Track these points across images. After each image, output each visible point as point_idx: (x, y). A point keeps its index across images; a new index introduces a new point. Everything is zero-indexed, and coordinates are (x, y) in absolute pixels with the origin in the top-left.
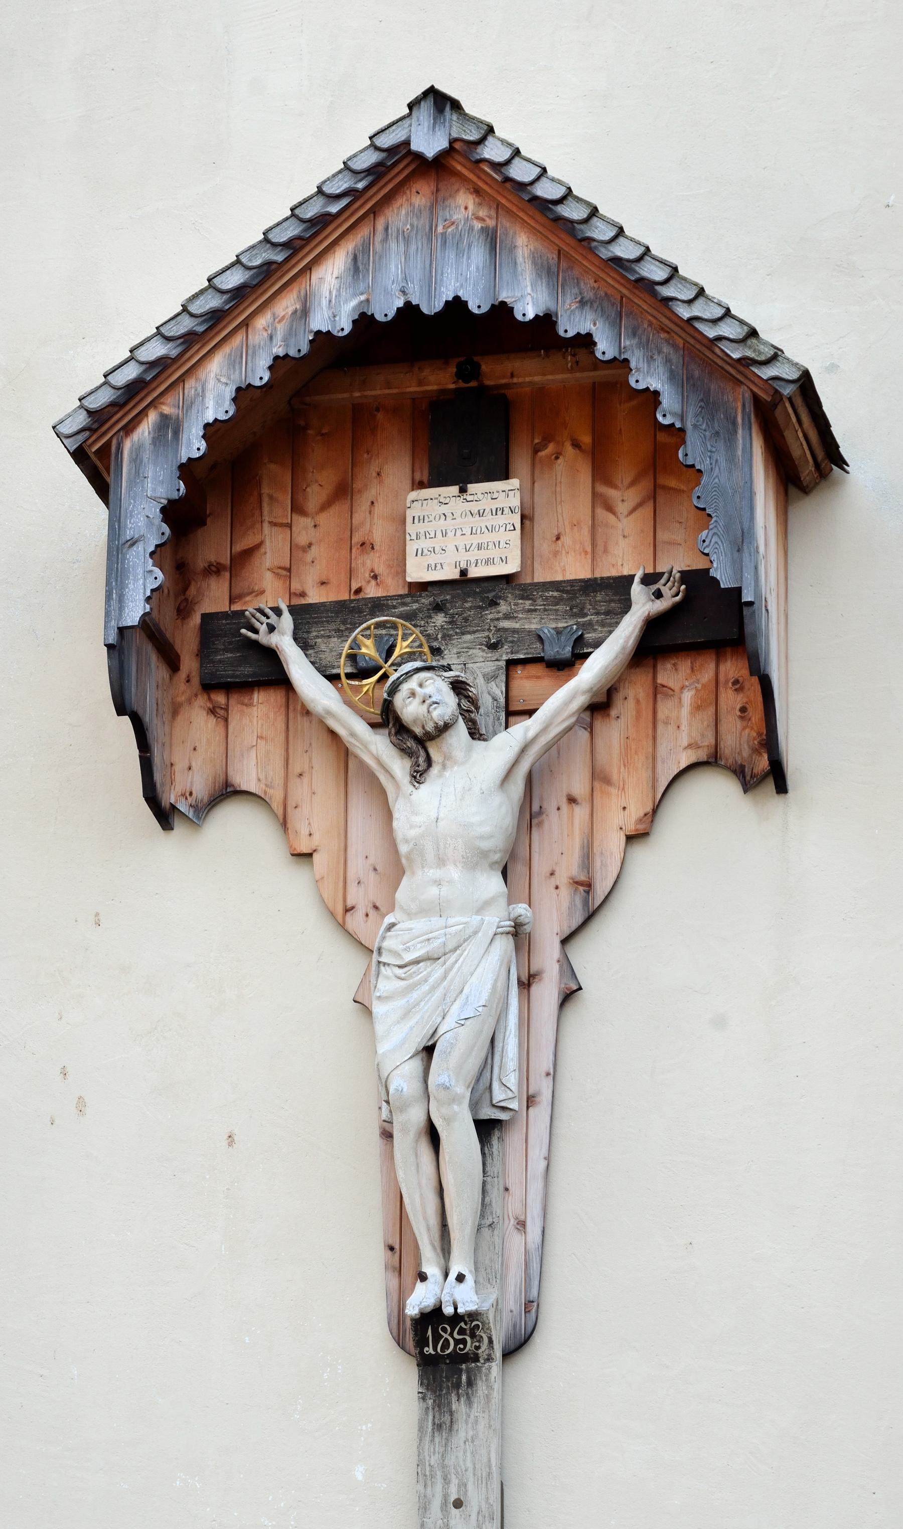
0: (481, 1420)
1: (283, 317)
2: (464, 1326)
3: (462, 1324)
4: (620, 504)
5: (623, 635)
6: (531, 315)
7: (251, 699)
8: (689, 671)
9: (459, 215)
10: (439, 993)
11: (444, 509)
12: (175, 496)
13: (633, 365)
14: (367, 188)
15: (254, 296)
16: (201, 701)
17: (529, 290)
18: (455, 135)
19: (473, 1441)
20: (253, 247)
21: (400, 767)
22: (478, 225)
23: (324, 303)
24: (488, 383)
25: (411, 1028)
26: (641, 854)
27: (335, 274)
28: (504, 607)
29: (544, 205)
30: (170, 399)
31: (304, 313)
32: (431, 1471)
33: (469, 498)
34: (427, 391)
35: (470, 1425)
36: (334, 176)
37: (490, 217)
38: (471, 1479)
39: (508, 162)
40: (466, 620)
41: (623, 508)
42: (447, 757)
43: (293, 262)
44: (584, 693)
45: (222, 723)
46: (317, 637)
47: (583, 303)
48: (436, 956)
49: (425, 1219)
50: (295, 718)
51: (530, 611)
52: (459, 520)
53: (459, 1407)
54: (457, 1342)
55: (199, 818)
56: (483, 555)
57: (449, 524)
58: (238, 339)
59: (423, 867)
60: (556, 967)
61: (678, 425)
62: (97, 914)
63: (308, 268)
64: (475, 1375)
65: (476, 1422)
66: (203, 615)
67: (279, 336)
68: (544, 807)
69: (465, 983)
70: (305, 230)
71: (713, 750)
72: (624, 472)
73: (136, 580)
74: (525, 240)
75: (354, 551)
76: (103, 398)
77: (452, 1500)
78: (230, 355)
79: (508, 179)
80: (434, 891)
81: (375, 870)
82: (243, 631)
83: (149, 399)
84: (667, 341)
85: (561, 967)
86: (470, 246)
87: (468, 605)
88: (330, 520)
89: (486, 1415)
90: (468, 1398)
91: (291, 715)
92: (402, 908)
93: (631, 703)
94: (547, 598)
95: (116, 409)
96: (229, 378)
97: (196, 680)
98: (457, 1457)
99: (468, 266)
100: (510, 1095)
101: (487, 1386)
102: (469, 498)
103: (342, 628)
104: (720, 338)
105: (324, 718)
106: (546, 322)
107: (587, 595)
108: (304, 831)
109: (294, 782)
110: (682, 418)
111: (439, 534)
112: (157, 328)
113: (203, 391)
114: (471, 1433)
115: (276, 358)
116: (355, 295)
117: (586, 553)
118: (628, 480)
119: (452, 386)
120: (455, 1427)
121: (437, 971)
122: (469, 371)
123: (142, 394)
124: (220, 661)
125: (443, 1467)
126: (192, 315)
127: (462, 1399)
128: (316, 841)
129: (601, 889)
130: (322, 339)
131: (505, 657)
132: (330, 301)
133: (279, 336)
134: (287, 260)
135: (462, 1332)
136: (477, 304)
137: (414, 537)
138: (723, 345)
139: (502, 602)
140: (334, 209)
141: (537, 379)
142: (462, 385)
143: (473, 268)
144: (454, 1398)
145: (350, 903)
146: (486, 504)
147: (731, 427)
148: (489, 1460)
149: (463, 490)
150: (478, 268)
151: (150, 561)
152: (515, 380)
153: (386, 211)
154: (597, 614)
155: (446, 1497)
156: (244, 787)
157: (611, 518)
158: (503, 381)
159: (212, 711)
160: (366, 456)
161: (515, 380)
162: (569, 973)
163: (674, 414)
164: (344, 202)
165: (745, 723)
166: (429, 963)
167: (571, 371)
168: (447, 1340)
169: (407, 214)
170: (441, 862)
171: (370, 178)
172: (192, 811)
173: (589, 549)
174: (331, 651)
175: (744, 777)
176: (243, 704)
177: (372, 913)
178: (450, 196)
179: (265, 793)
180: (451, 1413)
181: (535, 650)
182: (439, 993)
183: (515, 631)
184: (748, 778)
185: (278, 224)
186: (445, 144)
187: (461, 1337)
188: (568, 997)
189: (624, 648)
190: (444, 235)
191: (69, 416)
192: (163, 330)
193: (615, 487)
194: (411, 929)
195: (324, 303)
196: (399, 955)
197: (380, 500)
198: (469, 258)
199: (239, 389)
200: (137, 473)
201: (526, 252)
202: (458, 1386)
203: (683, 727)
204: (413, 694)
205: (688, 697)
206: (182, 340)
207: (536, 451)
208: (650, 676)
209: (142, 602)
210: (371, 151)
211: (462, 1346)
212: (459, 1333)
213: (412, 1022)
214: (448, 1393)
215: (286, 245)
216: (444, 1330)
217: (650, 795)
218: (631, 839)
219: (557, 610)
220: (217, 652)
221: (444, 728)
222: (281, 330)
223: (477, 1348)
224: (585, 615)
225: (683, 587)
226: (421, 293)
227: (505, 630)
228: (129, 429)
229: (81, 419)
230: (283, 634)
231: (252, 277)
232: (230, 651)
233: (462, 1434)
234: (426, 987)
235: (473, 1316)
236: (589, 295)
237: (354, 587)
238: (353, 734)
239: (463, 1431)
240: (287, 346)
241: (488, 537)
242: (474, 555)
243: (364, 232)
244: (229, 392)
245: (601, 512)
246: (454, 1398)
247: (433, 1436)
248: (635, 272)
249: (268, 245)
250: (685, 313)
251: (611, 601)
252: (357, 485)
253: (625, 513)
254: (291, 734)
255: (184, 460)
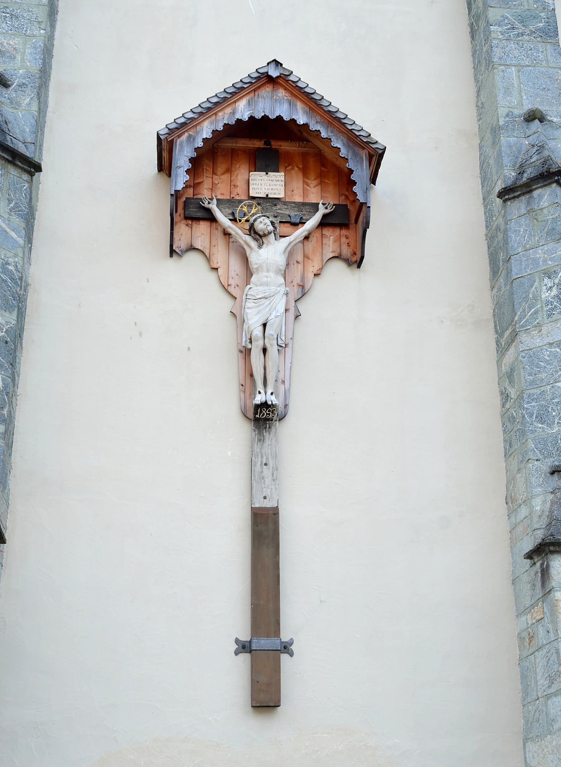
0: (273, 439)
1: (227, 113)
2: (270, 409)
3: (270, 409)
4: (311, 185)
5: (318, 217)
6: (302, 123)
7: (200, 223)
8: (332, 231)
9: (280, 95)
10: (268, 308)
11: (261, 178)
12: (193, 156)
13: (332, 140)
14: (255, 82)
15: (220, 106)
16: (184, 221)
17: (301, 116)
18: (281, 73)
19: (271, 445)
20: (221, 92)
21: (253, 244)
22: (286, 98)
23: (240, 111)
24: (273, 147)
25: (260, 317)
26: (318, 280)
27: (243, 104)
28: (278, 207)
29: (308, 95)
30: (192, 130)
31: (233, 113)
32: (257, 453)
33: (269, 176)
34: (254, 147)
35: (270, 440)
36: (245, 78)
37: (289, 96)
38: (270, 457)
39: (297, 81)
40: (267, 209)
41: (312, 186)
42: (269, 242)
43: (191, 123)
44: (307, 231)
45: (190, 229)
46: (222, 208)
47: (317, 122)
48: (267, 297)
49: (260, 375)
50: (213, 230)
51: (286, 208)
52: (266, 181)
53: (266, 434)
54: (267, 414)
55: (182, 254)
56: (273, 192)
57: (262, 182)
58: (214, 117)
59: (262, 272)
60: (294, 308)
61: (346, 157)
62: (148, 279)
63: (235, 102)
64: (271, 425)
65: (272, 439)
66: (186, 198)
67: (226, 118)
68: (289, 263)
69: (277, 306)
70: (237, 90)
71: (339, 253)
72: (312, 176)
73: (181, 177)
74: (300, 104)
75: (231, 187)
76: (173, 126)
77: (264, 463)
78: (211, 121)
79: (297, 86)
80: (265, 279)
81: (238, 275)
82: (201, 202)
83: (186, 129)
84: (342, 135)
85: (295, 308)
86: (283, 103)
87: (268, 205)
88: (226, 177)
89: (275, 438)
90: (269, 432)
91: (212, 229)
92: (253, 283)
93: (315, 238)
94: (291, 206)
95: (177, 130)
96: (210, 127)
97: (182, 216)
98: (265, 450)
99: (283, 108)
100: (283, 342)
101: (275, 429)
102: (269, 176)
103: (229, 206)
104: (360, 135)
105: (227, 228)
106: (306, 125)
107: (304, 206)
108: (215, 262)
109: (212, 248)
110: (347, 155)
111: (260, 184)
112: (191, 110)
113: (202, 129)
114: (270, 443)
115: (225, 124)
116: (249, 111)
117: (301, 196)
118: (313, 179)
119: (263, 147)
120: (265, 440)
121: (267, 302)
122: (267, 143)
123: (185, 127)
124: (191, 211)
125: (261, 453)
126: (202, 108)
127: (267, 432)
128: (219, 265)
129: (307, 288)
130: (239, 121)
131: (279, 220)
132: (241, 111)
133: (226, 118)
134: (230, 97)
135: (269, 411)
136: (286, 118)
137: (252, 184)
138: (361, 137)
139: (278, 205)
140: (245, 86)
141: (288, 148)
142: (265, 146)
143: (284, 108)
144: (264, 431)
145: (229, 283)
146: (274, 178)
147: (362, 160)
148: (276, 451)
149: (267, 174)
150: (286, 109)
151: (185, 173)
152: (281, 148)
153: (258, 91)
154: (306, 212)
155: (262, 462)
156: (197, 247)
157: (309, 188)
158: (278, 147)
159: (187, 225)
160: (235, 162)
161: (281, 148)
162: (297, 311)
163: (345, 154)
164: (248, 85)
165: (349, 247)
166: (264, 299)
167: (298, 147)
168: (264, 413)
169: (264, 92)
170: (268, 271)
171: (256, 80)
172: (180, 252)
173: (302, 195)
174: (226, 212)
175: (349, 262)
176: (197, 224)
177: (236, 287)
178: (277, 89)
179: (203, 250)
180: (264, 436)
181: (288, 219)
182: (268, 308)
183: (282, 213)
184: (350, 262)
185: (228, 88)
186: (279, 74)
187: (269, 413)
188: (297, 317)
189: (318, 220)
190: (276, 99)
191: (162, 129)
192: (226, 90)
193: (309, 180)
194: (258, 289)
195: (240, 111)
196: (255, 296)
197: (239, 174)
198: (283, 106)
199: (213, 131)
200: (181, 149)
201: (300, 107)
202: (266, 428)
203: (330, 246)
204: (261, 222)
205: (332, 238)
206: (198, 114)
207: (286, 167)
208: (321, 231)
209: (183, 184)
210: (257, 73)
211: (268, 416)
212: (268, 411)
213: (260, 315)
214: (262, 430)
215: (230, 93)
216: (264, 410)
217: (321, 264)
218: (315, 275)
219: (294, 209)
220: (190, 208)
221: (269, 233)
222: (226, 117)
223: (273, 417)
224: (303, 212)
225: (334, 207)
226: (269, 113)
227: (279, 213)
228: (179, 136)
229: (166, 131)
230: (214, 205)
231: (220, 100)
232: (195, 208)
233: (267, 443)
234: (264, 306)
235: (273, 405)
236: (319, 120)
237: (232, 196)
238: (237, 234)
239: (267, 442)
240: (228, 121)
241: (274, 187)
242: (270, 191)
243: (252, 95)
244: (211, 131)
245: (305, 186)
246: (264, 431)
247: (258, 443)
248: (334, 115)
249: (225, 93)
250: (350, 127)
251: (310, 209)
252: (233, 169)
253: (312, 187)
254: (212, 234)
255: (196, 147)
